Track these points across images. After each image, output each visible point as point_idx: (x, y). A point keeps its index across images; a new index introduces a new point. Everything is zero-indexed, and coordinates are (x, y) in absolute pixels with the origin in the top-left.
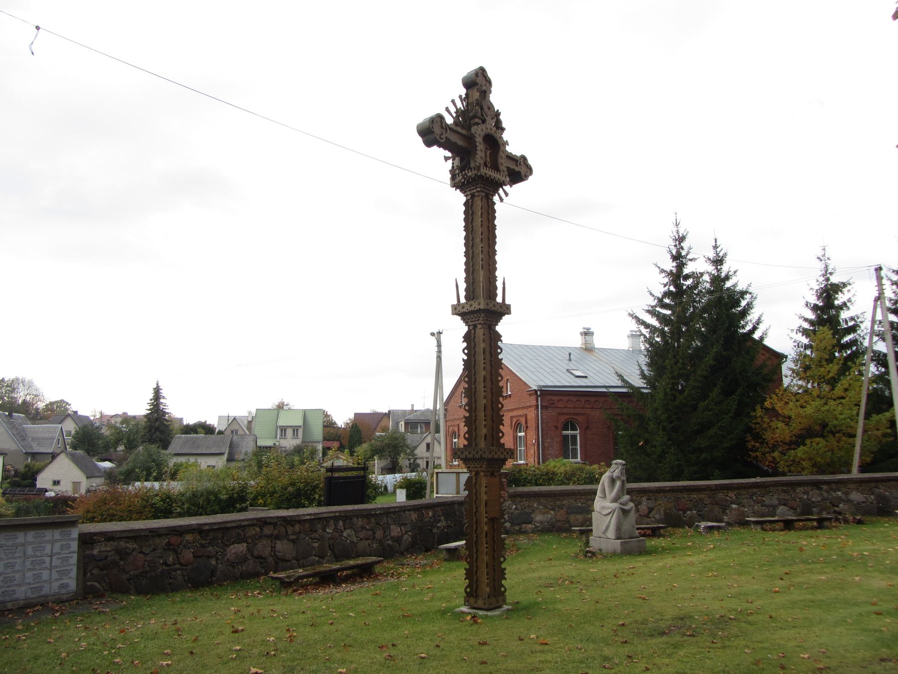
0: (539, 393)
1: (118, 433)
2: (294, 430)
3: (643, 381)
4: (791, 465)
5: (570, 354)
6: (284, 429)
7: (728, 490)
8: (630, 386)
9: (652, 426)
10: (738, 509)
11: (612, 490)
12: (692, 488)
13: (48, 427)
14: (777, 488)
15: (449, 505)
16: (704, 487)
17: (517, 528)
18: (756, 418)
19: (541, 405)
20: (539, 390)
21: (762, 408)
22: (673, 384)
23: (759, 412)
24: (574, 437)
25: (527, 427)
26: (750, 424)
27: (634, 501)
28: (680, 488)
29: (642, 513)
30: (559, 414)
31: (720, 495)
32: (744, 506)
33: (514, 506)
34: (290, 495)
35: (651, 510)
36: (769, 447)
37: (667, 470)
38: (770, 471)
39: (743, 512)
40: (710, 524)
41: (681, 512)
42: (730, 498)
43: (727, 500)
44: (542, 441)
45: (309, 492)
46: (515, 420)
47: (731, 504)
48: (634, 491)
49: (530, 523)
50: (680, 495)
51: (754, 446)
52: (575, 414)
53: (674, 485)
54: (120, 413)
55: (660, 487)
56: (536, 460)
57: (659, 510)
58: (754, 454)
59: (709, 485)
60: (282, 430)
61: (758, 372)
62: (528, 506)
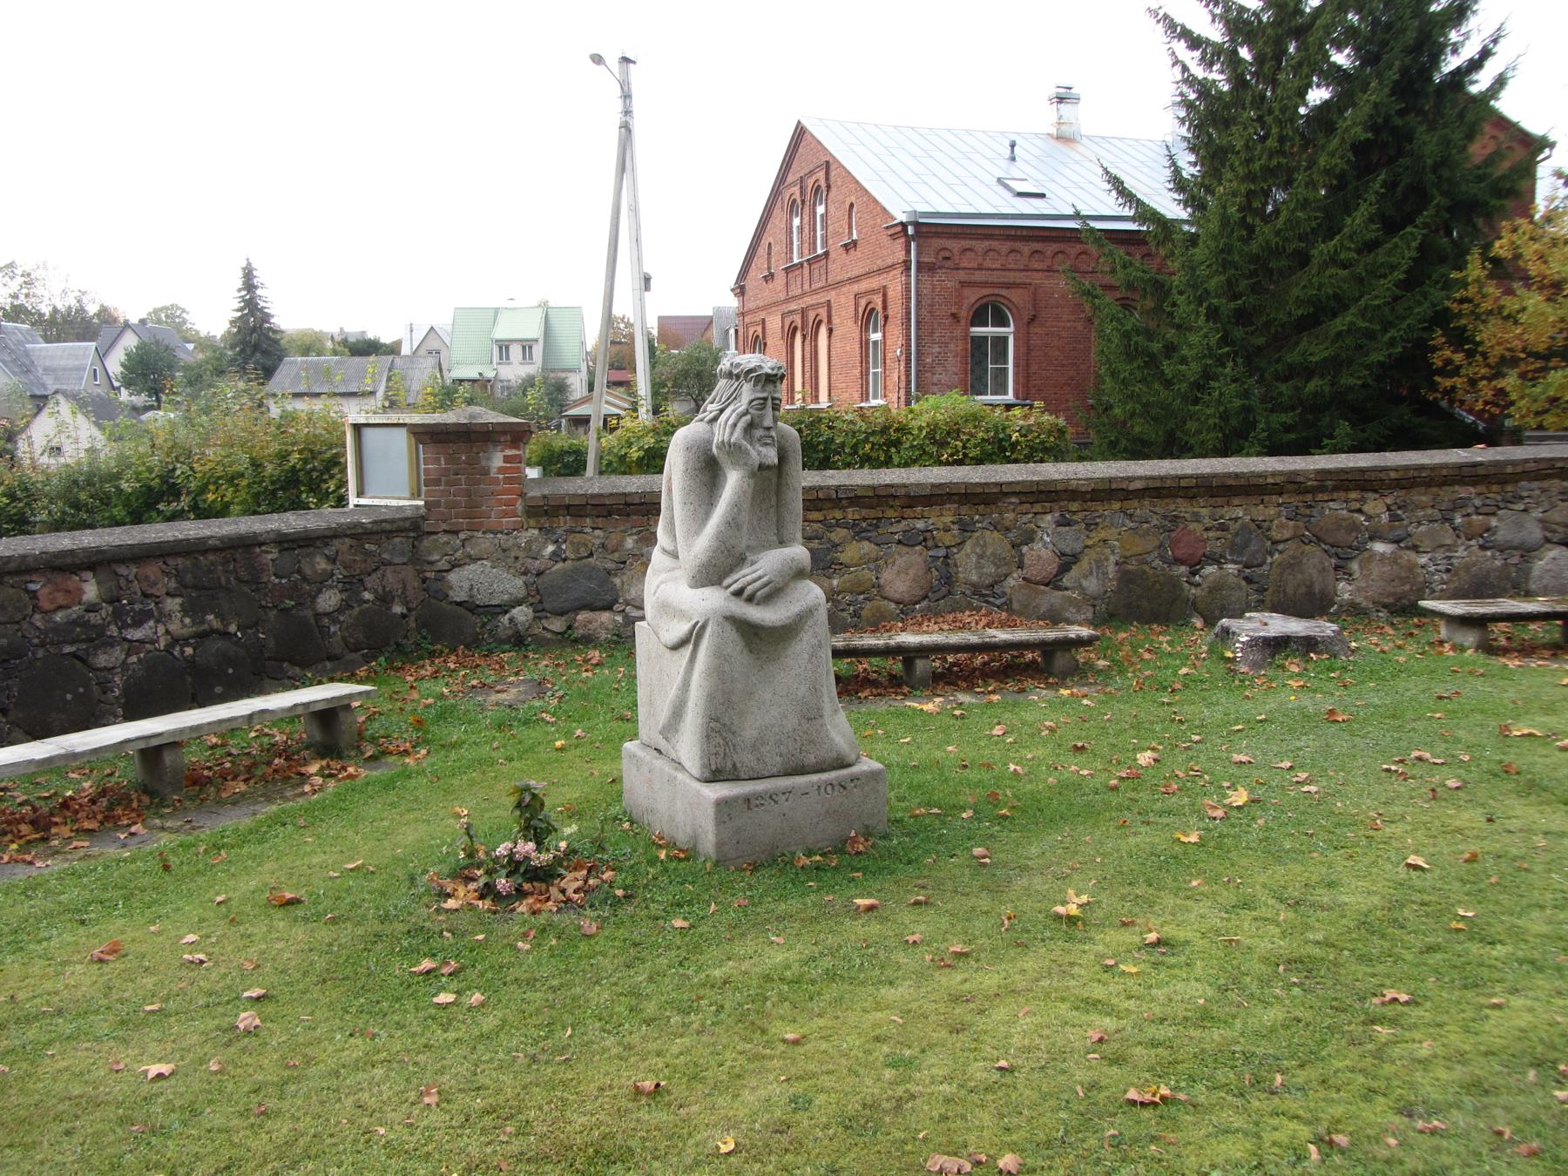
0: (910, 230)
1: (218, 359)
2: (524, 348)
3: (1176, 196)
4: (1546, 411)
5: (1013, 146)
6: (504, 347)
7: (1364, 490)
8: (1145, 213)
9: (1183, 306)
10: (1394, 559)
11: (698, 532)
12: (1230, 482)
13: (72, 348)
14: (1546, 484)
15: (215, 550)
16: (1278, 480)
17: (557, 625)
18: (1464, 284)
19: (918, 262)
20: (911, 223)
21: (1485, 257)
22: (1250, 194)
23: (1475, 269)
24: (1001, 342)
25: (886, 318)
26: (1447, 303)
27: (1008, 529)
28: (1183, 483)
29: (1034, 572)
30: (963, 284)
31: (1335, 509)
32: (1415, 548)
33: (551, 548)
34: (273, 483)
35: (1067, 562)
36: (1488, 365)
37: (1211, 421)
38: (1481, 426)
39: (1411, 567)
40: (1279, 625)
41: (1183, 569)
42: (1369, 518)
43: (1355, 527)
44: (918, 351)
45: (315, 475)
46: (863, 302)
47: (1372, 539)
48: (1007, 494)
49: (608, 607)
50: (1183, 508)
51: (1448, 362)
52: (1007, 286)
53: (1163, 472)
54: (132, 310)
55: (1111, 480)
56: (903, 398)
57: (1099, 564)
58: (1448, 383)
59: (1295, 473)
60: (501, 348)
61: (1481, 172)
62: (603, 545)
